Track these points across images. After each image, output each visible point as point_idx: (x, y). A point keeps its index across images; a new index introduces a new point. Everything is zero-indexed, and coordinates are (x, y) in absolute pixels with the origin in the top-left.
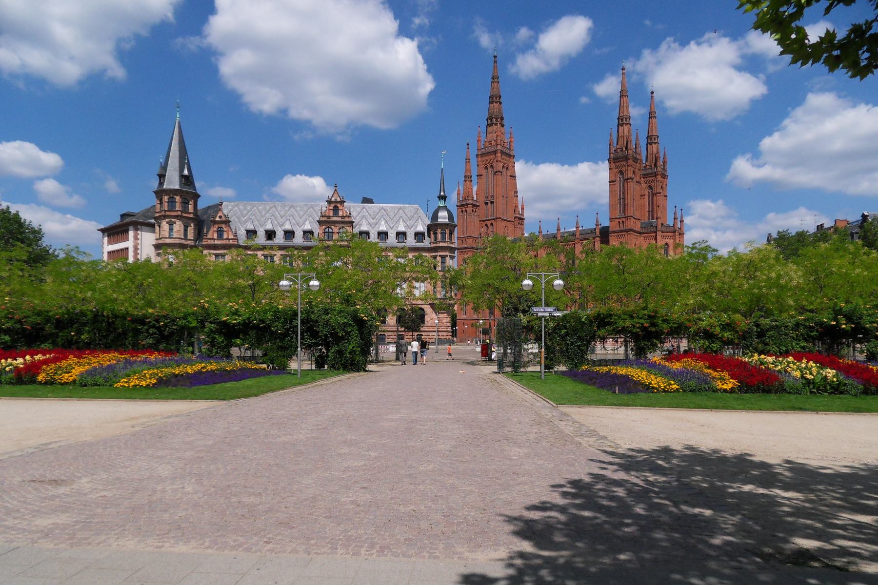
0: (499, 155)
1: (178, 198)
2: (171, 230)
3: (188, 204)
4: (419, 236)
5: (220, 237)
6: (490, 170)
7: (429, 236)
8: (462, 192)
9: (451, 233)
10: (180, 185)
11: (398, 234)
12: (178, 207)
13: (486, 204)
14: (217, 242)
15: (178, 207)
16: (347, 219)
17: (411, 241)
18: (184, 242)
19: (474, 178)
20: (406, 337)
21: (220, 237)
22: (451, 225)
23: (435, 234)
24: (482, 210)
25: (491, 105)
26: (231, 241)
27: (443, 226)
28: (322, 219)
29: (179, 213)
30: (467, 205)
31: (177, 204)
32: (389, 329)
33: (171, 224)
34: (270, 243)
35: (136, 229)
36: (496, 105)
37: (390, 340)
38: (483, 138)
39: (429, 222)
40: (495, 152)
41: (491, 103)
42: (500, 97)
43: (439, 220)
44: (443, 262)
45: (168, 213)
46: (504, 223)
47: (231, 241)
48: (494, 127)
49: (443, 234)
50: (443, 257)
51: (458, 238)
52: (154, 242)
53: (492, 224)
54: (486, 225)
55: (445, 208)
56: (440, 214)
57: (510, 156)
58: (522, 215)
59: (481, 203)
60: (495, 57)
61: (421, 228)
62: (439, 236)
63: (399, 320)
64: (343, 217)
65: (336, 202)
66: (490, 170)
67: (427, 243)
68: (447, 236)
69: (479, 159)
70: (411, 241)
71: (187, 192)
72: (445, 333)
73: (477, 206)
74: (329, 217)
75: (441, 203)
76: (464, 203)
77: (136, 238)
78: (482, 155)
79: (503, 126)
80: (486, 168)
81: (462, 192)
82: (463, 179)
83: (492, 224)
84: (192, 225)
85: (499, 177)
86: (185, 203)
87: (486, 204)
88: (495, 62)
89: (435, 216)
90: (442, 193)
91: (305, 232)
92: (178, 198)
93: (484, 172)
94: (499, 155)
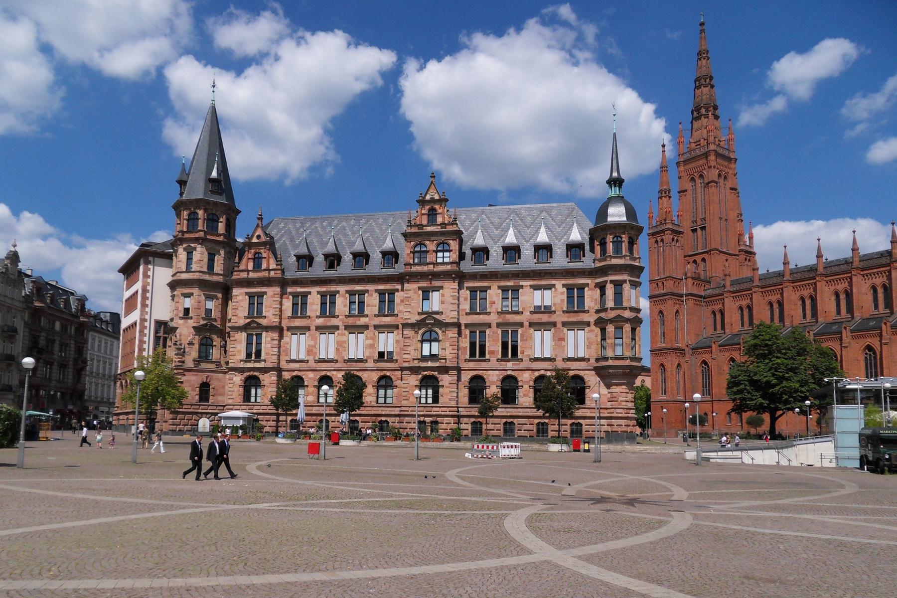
0: (712, 157)
1: (201, 213)
2: (189, 259)
3: (217, 221)
4: (574, 249)
5: (257, 267)
6: (698, 181)
7: (592, 250)
8: (655, 215)
9: (631, 243)
10: (205, 193)
11: (538, 248)
12: (201, 225)
13: (694, 231)
14: (252, 275)
15: (201, 225)
16: (449, 228)
17: (560, 260)
18: (207, 277)
19: (674, 194)
20: (550, 428)
21: (257, 267)
22: (632, 227)
23: (603, 245)
24: (687, 239)
25: (698, 92)
26: (272, 273)
27: (617, 228)
28: (409, 230)
29: (202, 234)
30: (663, 231)
31: (200, 222)
32: (521, 412)
33: (190, 254)
34: (331, 273)
35: (147, 263)
36: (706, 90)
37: (523, 433)
38: (687, 138)
39: (591, 226)
40: (706, 155)
41: (697, 88)
42: (711, 78)
43: (610, 219)
44: (618, 295)
45: (187, 236)
46: (724, 257)
47: (272, 273)
48: (704, 121)
49: (617, 244)
50: (618, 285)
51: (651, 281)
52: (170, 279)
53: (704, 260)
54: (695, 262)
55: (620, 199)
56: (611, 210)
57: (729, 160)
58: (751, 246)
59: (686, 227)
60: (702, 24)
61: (576, 235)
62: (610, 247)
63: (539, 401)
64: (443, 225)
65: (433, 201)
66: (698, 181)
67: (588, 261)
68: (625, 246)
69: (682, 168)
70: (560, 260)
71: (215, 203)
72: (623, 422)
73: (679, 233)
74: (421, 226)
75: (614, 192)
76: (660, 229)
77: (146, 276)
78: (686, 162)
79: (717, 117)
80: (693, 179)
81: (655, 215)
82: (658, 195)
83: (704, 260)
84: (222, 252)
85: (713, 190)
86: (212, 221)
87: (694, 231)
88: (702, 31)
89: (602, 213)
90: (615, 174)
91: (384, 254)
92: (201, 213)
93: (688, 186)
94: (712, 157)
